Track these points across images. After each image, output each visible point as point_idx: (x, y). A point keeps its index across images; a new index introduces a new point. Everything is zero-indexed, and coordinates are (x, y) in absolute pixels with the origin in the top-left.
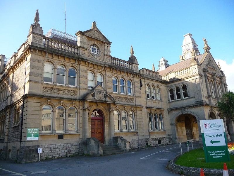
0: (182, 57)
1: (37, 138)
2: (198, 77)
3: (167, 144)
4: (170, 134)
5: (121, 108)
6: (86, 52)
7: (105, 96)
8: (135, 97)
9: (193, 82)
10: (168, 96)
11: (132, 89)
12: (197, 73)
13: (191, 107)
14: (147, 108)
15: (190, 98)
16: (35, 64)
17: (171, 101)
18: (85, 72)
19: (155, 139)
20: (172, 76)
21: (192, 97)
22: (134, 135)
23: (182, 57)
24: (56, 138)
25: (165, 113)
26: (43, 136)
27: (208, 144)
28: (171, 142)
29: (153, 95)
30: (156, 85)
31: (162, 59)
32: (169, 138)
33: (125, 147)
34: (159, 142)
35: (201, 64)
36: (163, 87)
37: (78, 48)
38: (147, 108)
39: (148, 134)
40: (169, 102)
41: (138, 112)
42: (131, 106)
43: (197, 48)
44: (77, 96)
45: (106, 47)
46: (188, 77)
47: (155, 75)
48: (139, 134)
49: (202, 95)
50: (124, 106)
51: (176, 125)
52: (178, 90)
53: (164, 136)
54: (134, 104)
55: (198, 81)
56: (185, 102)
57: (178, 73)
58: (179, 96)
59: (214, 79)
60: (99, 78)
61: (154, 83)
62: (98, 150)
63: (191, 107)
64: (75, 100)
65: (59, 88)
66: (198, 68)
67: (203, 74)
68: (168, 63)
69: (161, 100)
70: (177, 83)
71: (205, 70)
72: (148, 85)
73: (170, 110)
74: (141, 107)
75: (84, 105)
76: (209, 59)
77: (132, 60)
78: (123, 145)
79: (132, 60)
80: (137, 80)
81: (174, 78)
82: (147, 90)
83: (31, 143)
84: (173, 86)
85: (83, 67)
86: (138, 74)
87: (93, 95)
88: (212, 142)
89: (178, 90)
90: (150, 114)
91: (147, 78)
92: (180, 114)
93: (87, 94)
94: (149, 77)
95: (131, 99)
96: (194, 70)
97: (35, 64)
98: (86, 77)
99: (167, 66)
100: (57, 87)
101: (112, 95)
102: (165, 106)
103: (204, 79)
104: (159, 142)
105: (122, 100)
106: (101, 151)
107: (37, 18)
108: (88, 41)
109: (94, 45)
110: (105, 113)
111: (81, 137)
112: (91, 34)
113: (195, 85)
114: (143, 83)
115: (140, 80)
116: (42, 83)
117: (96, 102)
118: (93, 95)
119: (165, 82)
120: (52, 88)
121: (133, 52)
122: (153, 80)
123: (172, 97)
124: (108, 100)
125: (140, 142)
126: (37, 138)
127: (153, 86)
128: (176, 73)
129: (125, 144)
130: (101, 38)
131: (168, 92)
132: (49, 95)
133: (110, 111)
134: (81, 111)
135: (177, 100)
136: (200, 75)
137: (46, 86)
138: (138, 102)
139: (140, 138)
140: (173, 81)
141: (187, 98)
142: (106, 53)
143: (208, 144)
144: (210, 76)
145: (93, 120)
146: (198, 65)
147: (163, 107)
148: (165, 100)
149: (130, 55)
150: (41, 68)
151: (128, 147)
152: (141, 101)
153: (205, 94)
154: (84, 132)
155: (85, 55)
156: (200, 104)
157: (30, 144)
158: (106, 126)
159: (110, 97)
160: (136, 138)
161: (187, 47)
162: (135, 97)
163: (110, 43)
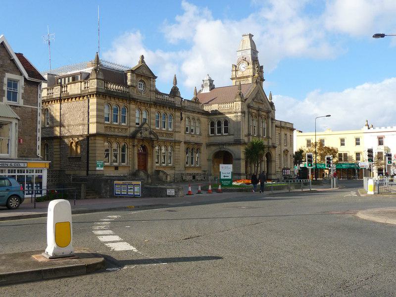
0: (236, 67)
1: (102, 169)
2: (240, 114)
3: (202, 180)
4: (205, 170)
5: (162, 143)
6: (135, 90)
7: (151, 133)
8: (175, 132)
9: (234, 119)
10: (208, 129)
11: (172, 124)
12: (240, 110)
13: (229, 144)
14: (185, 143)
15: (230, 135)
16: (100, 107)
17: (210, 135)
18: (134, 110)
19: (190, 174)
20: (214, 107)
21: (232, 135)
22: (172, 169)
23: (236, 67)
24: (113, 169)
25: (203, 149)
26: (105, 167)
27: (222, 177)
28: (206, 178)
29: (192, 128)
30: (196, 118)
31: (208, 78)
32: (204, 174)
33: (167, 179)
34: (194, 177)
35: (246, 100)
36: (204, 119)
37: (128, 87)
38: (185, 143)
39: (183, 169)
40: (209, 136)
41: (176, 147)
42: (171, 142)
43: (257, 58)
44: (128, 134)
45: (152, 82)
46: (230, 113)
47: (197, 106)
48: (176, 169)
49: (242, 134)
50: (165, 141)
51: (213, 162)
52: (219, 124)
53: (200, 172)
54: (173, 139)
55: (239, 119)
56: (225, 138)
57: (222, 105)
58: (219, 131)
59: (259, 115)
60: (144, 116)
61: (195, 115)
62: (148, 180)
63: (229, 144)
64: (126, 137)
65: (115, 126)
66: (242, 104)
67: (246, 110)
68: (214, 83)
69: (200, 135)
70: (219, 116)
71: (249, 107)
72: (188, 118)
73: (209, 145)
74: (179, 142)
75: (133, 141)
76: (258, 91)
77: (175, 92)
78: (164, 178)
79: (175, 92)
80: (178, 114)
81: (216, 110)
82: (187, 123)
83: (99, 172)
84: (215, 118)
85: (133, 106)
86: (181, 109)
87: (141, 133)
88: (224, 176)
89: (219, 124)
90: (187, 149)
91: (188, 111)
92: (217, 150)
93: (136, 132)
94: (191, 109)
95: (170, 134)
96: (238, 106)
97: (100, 107)
98: (134, 116)
99: (212, 87)
100: (113, 126)
101: (154, 131)
102: (203, 140)
103: (247, 116)
104: (194, 177)
105: (163, 136)
106: (150, 181)
107: (175, 82)
108: (137, 77)
109: (141, 81)
110: (149, 148)
111: (130, 169)
112: (140, 71)
113: (238, 123)
114: (183, 116)
115: (181, 113)
116: (104, 124)
117: (143, 140)
118: (141, 133)
119: (206, 113)
120: (110, 127)
121: (176, 82)
122: (194, 112)
123: (213, 131)
124: (152, 136)
125: (176, 176)
126: (102, 169)
127: (194, 119)
128: (220, 106)
129: (167, 177)
130: (148, 73)
131: (208, 124)
132: (109, 133)
133: (153, 147)
134: (131, 147)
135: (217, 135)
136: (243, 112)
137: (106, 125)
138: (177, 137)
139: (43, 195)
140: (216, 113)
141: (227, 134)
142: (152, 89)
143: (222, 177)
144: (255, 111)
145: (139, 154)
146: (242, 101)
147: (201, 142)
148: (204, 134)
149: (172, 85)
150: (102, 111)
151: (169, 179)
152: (181, 136)
153: (244, 132)
154: (133, 164)
155: (134, 93)
156: (238, 142)
157: (99, 173)
158: (149, 160)
159: (154, 134)
160: (173, 172)
161: (244, 54)
162: (175, 132)
163: (156, 77)
